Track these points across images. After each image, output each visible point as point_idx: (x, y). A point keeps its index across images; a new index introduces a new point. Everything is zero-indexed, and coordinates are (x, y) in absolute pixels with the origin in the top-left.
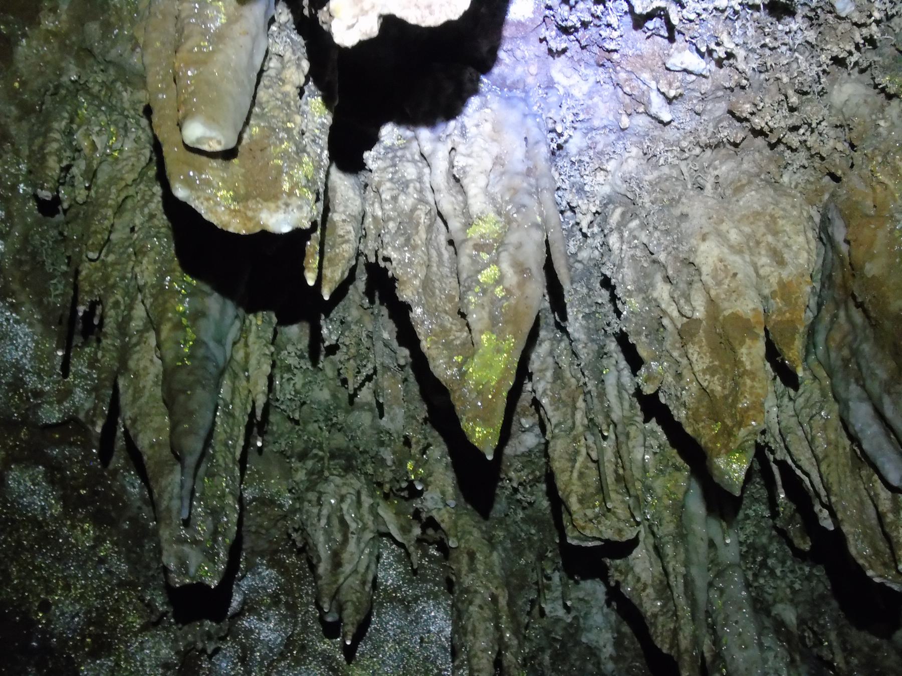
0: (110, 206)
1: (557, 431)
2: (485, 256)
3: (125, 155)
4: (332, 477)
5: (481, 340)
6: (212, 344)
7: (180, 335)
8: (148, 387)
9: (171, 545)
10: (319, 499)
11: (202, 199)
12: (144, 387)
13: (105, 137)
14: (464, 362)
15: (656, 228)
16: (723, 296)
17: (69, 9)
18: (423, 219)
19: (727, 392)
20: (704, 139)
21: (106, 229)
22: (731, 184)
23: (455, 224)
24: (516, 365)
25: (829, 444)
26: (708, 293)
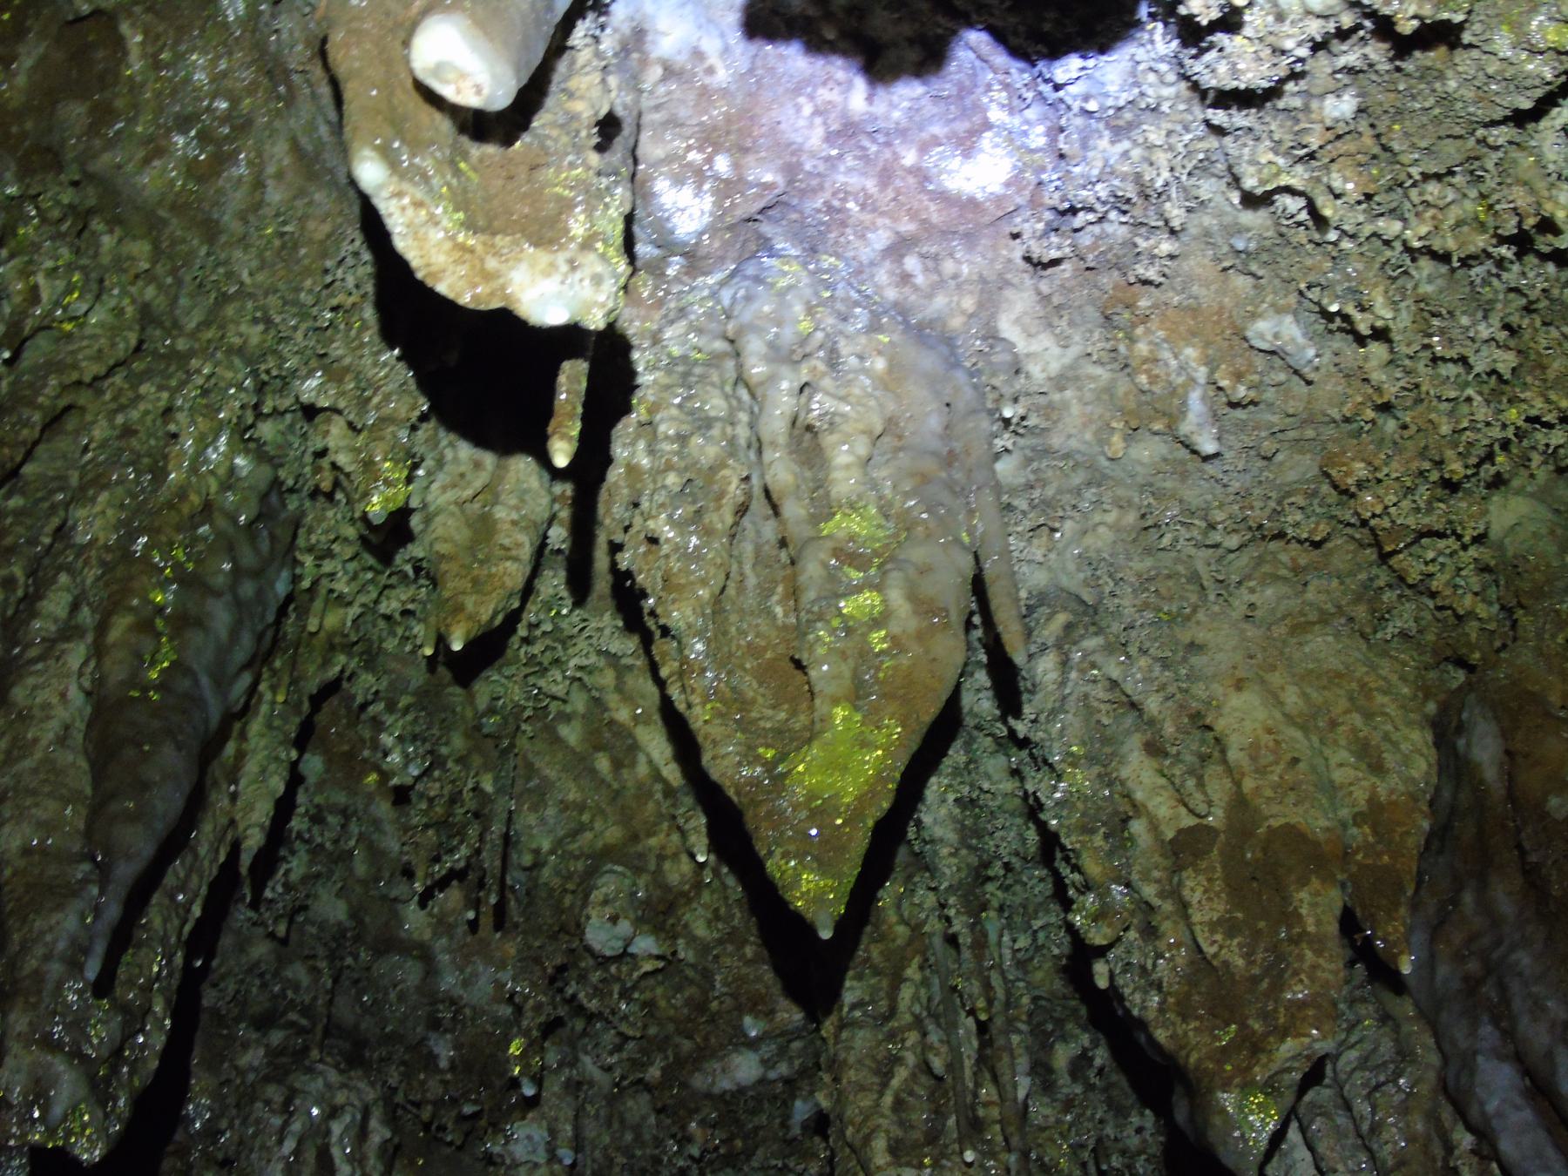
0: (40, 407)
1: (858, 1014)
2: (856, 576)
3: (88, 331)
4: (321, 1067)
5: (831, 717)
6: (205, 681)
7: (147, 644)
8: (44, 742)
9: (27, 1046)
10: (288, 1101)
11: (406, 201)
12: (36, 741)
13: (60, 284)
14: (782, 757)
15: (1144, 652)
16: (1269, 793)
17: (34, 68)
18: (734, 490)
19: (1256, 971)
20: (1257, 515)
21: (24, 443)
22: (1284, 618)
23: (793, 510)
24: (898, 775)
25: (1411, 1140)
26: (1238, 784)
